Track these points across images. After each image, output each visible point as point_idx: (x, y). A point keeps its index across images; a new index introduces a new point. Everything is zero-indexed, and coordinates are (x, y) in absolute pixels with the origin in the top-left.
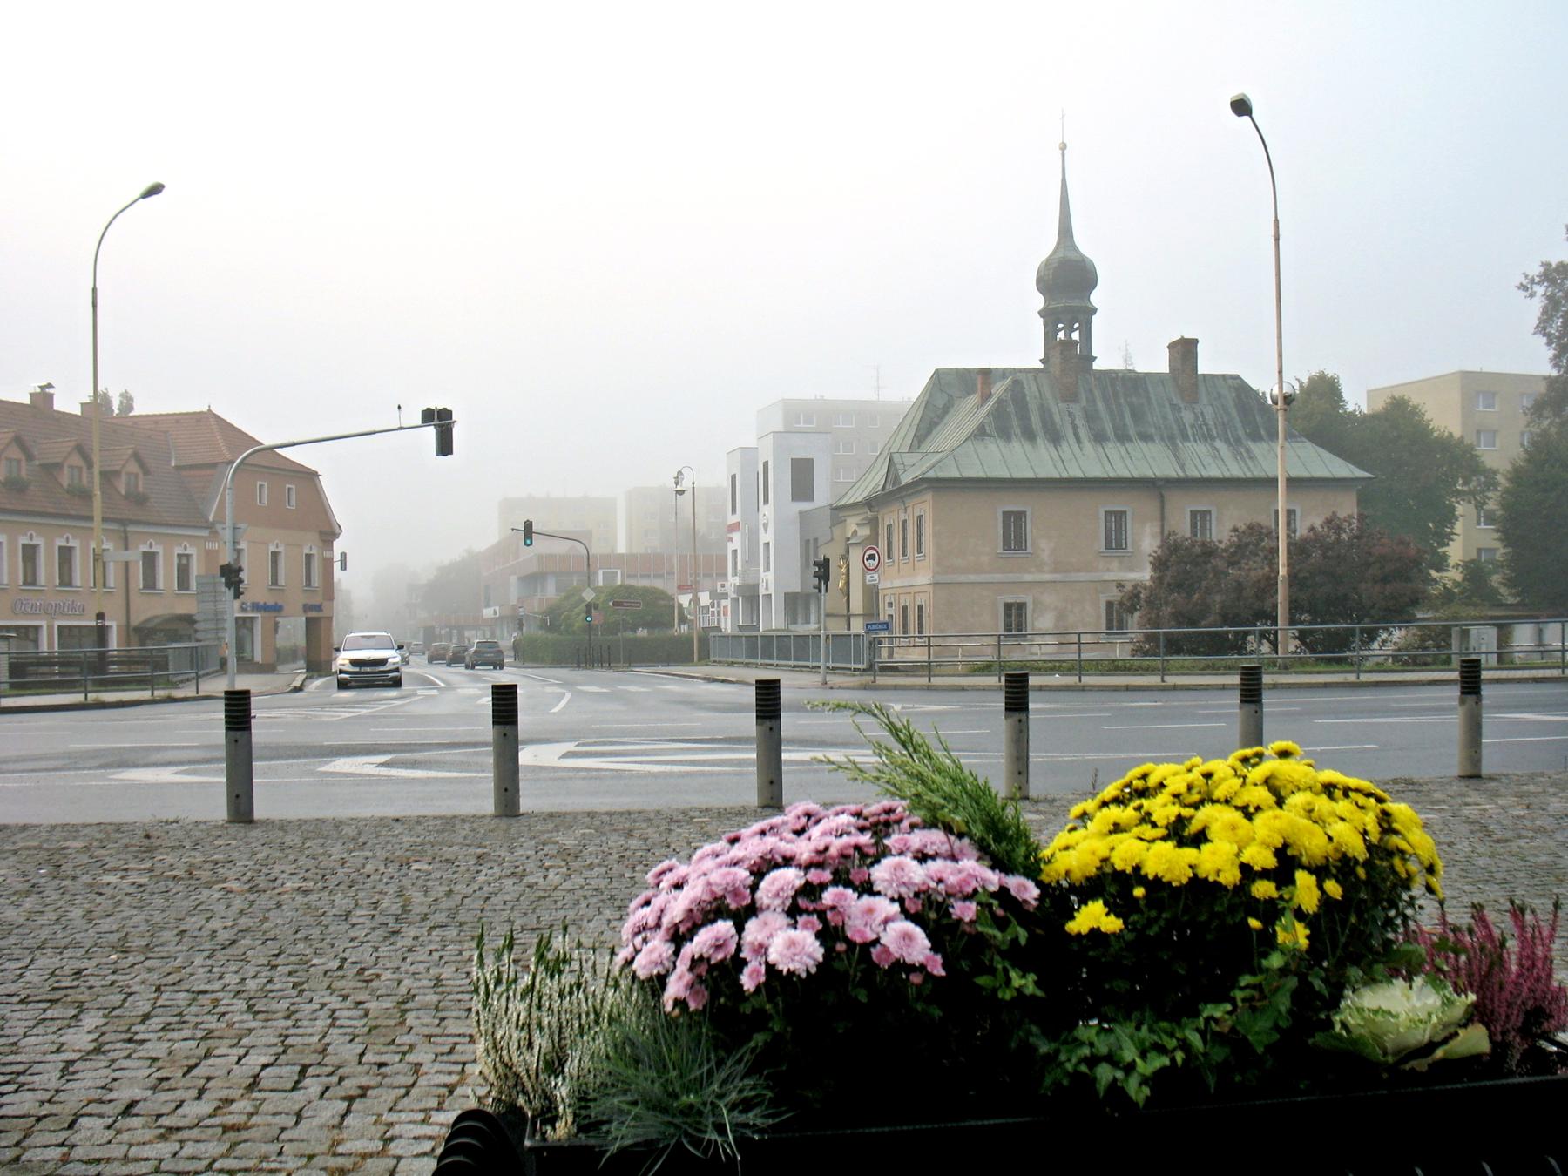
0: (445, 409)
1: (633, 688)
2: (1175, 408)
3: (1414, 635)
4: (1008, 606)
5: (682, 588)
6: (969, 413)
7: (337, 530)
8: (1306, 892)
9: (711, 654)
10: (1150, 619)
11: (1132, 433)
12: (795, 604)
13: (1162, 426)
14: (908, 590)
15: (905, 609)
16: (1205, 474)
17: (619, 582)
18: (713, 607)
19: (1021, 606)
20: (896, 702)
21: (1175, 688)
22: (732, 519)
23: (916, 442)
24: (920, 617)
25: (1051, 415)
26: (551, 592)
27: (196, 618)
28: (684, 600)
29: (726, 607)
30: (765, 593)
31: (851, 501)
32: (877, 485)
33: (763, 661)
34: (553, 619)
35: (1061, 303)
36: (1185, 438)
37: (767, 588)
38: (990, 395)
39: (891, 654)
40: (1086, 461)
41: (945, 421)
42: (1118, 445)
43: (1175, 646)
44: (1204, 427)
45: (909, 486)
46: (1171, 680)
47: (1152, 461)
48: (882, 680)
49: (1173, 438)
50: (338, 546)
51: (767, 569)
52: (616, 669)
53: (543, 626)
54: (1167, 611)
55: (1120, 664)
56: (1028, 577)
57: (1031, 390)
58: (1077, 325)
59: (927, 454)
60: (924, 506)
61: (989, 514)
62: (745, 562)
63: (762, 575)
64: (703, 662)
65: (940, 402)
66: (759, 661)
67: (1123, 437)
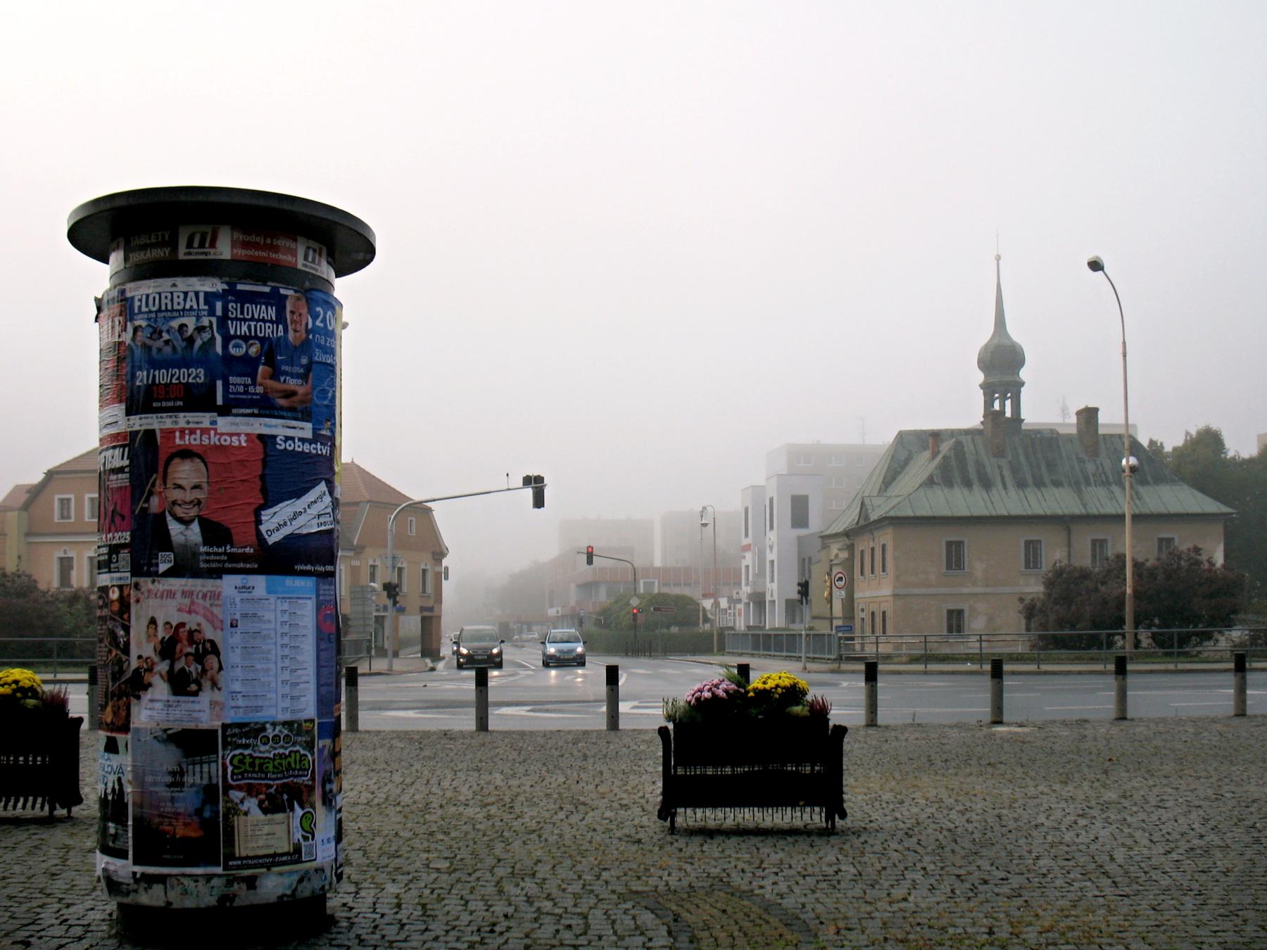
0: (539, 476)
1: (669, 671)
2: (1080, 460)
3: (1247, 635)
4: (950, 612)
5: (705, 596)
6: (923, 466)
7: (446, 551)
8: (779, 690)
9: (727, 646)
10: (1041, 624)
11: (1047, 480)
12: (792, 608)
13: (1070, 475)
14: (874, 600)
15: (873, 614)
16: (1102, 511)
17: (656, 591)
18: (730, 608)
19: (960, 613)
20: (845, 681)
21: (1046, 673)
22: (745, 542)
23: (883, 487)
24: (884, 620)
25: (984, 467)
26: (602, 597)
27: (349, 617)
28: (707, 604)
29: (740, 610)
30: (770, 599)
31: (834, 532)
32: (854, 520)
33: (775, 653)
34: (605, 618)
35: (994, 379)
36: (1088, 484)
37: (772, 596)
38: (939, 452)
39: (863, 649)
40: (1010, 502)
41: (906, 471)
42: (1036, 490)
43: (1059, 643)
44: (1103, 475)
45: (876, 522)
46: (1044, 667)
47: (1060, 501)
48: (844, 667)
49: (1078, 484)
50: (445, 562)
51: (772, 581)
52: (656, 657)
53: (598, 623)
54: (1052, 617)
55: (1015, 656)
56: (965, 590)
57: (969, 448)
58: (1009, 395)
59: (890, 497)
60: (886, 537)
61: (938, 541)
62: (755, 575)
63: (768, 585)
64: (721, 653)
65: (903, 455)
66: (761, 652)
67: (1039, 484)
